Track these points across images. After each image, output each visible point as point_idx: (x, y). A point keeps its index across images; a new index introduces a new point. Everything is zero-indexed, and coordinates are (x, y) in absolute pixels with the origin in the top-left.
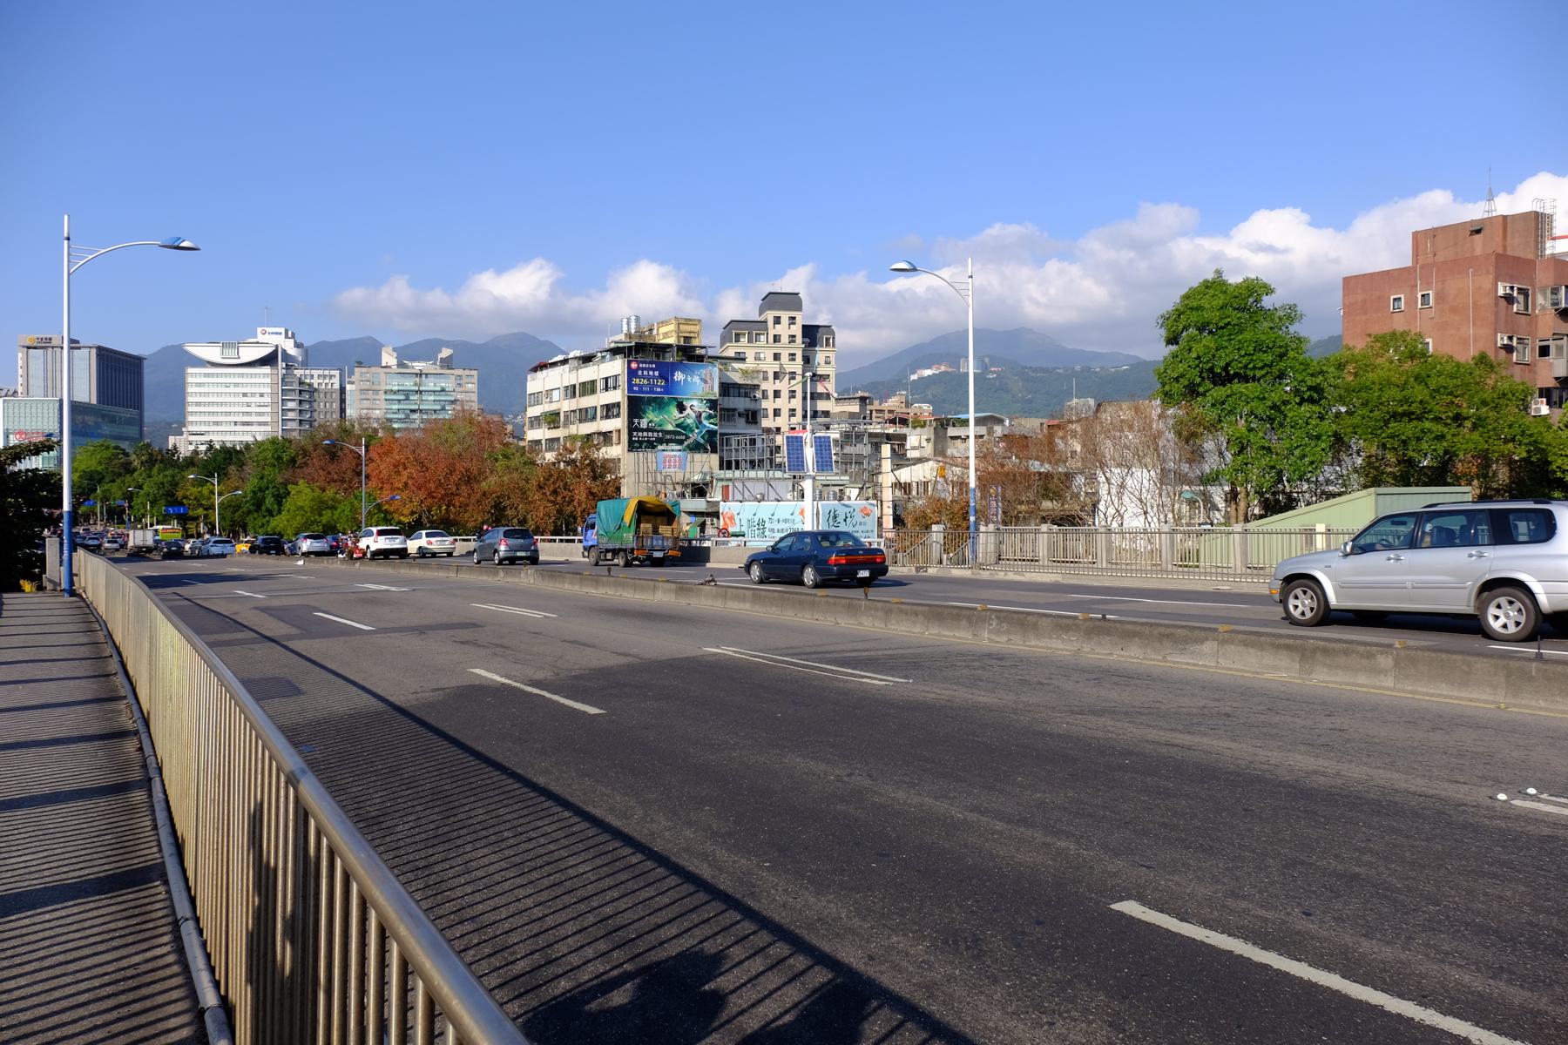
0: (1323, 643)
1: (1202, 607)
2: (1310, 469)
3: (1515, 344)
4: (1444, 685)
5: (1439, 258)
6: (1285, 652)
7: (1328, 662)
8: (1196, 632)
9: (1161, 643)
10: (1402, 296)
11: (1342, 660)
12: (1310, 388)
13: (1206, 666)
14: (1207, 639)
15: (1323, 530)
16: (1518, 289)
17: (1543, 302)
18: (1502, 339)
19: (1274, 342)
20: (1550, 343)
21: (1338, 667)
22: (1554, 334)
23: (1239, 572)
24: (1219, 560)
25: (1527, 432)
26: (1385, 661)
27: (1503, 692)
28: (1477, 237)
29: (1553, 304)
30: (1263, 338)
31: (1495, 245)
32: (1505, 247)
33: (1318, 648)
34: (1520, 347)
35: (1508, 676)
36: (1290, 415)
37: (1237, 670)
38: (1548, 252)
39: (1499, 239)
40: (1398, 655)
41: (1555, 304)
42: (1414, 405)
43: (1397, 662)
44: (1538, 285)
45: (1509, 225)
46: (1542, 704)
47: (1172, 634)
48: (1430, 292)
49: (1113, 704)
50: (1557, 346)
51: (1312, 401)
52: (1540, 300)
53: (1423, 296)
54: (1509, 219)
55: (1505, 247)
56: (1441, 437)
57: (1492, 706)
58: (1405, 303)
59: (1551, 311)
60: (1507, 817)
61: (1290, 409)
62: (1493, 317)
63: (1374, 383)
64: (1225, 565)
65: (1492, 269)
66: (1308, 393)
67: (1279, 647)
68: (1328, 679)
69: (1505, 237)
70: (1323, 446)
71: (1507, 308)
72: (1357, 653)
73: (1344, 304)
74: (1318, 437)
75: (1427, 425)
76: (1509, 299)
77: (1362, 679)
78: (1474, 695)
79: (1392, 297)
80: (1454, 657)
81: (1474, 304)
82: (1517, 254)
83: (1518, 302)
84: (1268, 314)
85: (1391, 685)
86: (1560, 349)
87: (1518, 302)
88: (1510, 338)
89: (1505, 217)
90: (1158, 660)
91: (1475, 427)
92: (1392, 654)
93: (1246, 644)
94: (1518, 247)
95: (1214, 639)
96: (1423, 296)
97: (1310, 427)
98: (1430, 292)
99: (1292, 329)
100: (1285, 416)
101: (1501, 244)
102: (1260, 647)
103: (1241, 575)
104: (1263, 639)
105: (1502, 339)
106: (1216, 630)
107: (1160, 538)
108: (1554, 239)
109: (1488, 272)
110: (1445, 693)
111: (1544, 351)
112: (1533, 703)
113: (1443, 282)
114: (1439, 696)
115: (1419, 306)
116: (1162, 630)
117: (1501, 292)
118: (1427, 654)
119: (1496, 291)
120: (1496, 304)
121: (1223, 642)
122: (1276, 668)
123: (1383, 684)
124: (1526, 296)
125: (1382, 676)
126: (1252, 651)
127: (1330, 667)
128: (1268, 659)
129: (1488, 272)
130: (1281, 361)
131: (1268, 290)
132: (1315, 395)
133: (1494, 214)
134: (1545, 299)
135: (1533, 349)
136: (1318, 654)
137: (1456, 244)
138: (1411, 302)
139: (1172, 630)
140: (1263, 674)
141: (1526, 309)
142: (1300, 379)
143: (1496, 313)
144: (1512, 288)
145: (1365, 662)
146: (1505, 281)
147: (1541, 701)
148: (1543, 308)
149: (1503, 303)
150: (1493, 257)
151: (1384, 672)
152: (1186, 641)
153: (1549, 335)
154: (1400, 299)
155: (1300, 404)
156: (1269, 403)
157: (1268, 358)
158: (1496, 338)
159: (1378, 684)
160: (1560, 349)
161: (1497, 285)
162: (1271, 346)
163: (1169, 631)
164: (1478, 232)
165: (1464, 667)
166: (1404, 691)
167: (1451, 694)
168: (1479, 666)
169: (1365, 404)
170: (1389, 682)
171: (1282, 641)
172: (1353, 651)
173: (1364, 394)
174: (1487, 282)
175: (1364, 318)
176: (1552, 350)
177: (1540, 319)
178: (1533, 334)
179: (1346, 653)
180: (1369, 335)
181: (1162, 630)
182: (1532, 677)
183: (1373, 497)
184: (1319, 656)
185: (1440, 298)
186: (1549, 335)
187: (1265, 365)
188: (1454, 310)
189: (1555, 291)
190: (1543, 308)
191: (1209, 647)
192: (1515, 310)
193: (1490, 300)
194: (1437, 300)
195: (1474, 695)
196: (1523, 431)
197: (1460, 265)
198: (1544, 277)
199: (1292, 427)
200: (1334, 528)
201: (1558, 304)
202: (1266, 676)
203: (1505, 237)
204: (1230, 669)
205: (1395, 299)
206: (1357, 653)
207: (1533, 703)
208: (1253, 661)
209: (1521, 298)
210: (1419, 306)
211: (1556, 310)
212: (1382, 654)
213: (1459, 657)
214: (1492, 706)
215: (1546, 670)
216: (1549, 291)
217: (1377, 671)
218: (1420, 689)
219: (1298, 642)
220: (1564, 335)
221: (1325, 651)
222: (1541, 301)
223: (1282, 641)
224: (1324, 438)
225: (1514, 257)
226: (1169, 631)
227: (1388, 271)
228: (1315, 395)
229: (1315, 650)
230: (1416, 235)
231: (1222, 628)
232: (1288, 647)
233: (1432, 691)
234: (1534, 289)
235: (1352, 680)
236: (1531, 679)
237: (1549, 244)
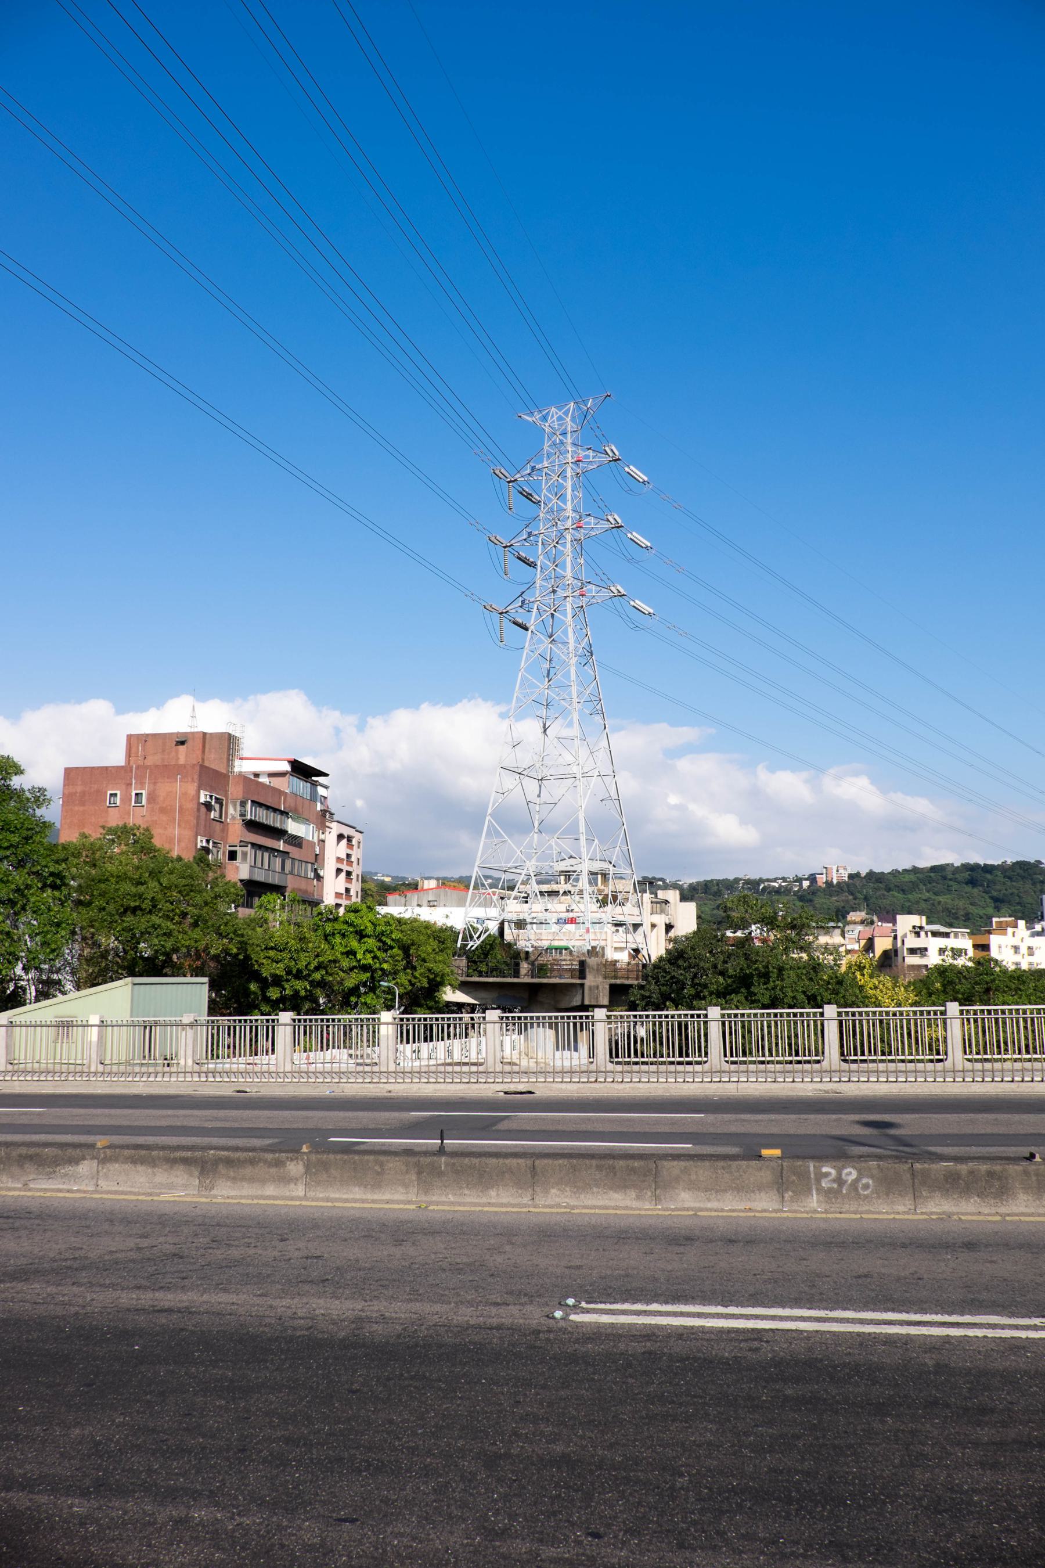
0: (226, 1153)
1: (536, 1119)
2: (51, 957)
3: (211, 847)
4: (357, 1189)
5: (149, 762)
6: (182, 1167)
7: (232, 1174)
8: (70, 1151)
9: (21, 1166)
10: (118, 792)
11: (248, 1171)
12: (52, 874)
13: (85, 1192)
14: (84, 1159)
15: (97, 1022)
16: (216, 798)
17: (233, 813)
18: (202, 841)
19: (23, 824)
20: (238, 849)
21: (243, 1179)
22: (241, 841)
23: (93, 1069)
24: (79, 1056)
25: (239, 932)
26: (295, 1168)
27: (415, 1190)
28: (181, 748)
29: (241, 815)
30: (12, 817)
31: (196, 758)
32: (203, 759)
33: (220, 1159)
34: (215, 850)
35: (419, 1173)
36: (32, 899)
37: (122, 1193)
38: (236, 770)
39: (199, 753)
40: (308, 1160)
41: (243, 815)
42: (146, 901)
43: (308, 1167)
44: (230, 797)
45: (207, 741)
46: (451, 1198)
47: (37, 1155)
48: (143, 792)
49: (23, 1261)
50: (242, 852)
51: (54, 887)
52: (231, 810)
53: (137, 794)
54: (208, 736)
55: (203, 759)
56: (168, 934)
57: (413, 1207)
58: (121, 800)
59: (239, 821)
60: (563, 1330)
61: (32, 894)
62: (195, 821)
63: (112, 876)
64: (78, 1062)
65: (196, 777)
66: (51, 879)
67: (173, 1162)
68: (232, 1193)
69: (203, 752)
70: (63, 933)
71: (206, 814)
72: (265, 1161)
73: (64, 794)
74: (58, 925)
75: (156, 919)
76: (208, 806)
77: (270, 1190)
78: (387, 1196)
79: (109, 792)
80: (366, 1157)
81: (180, 807)
82: (213, 766)
83: (215, 810)
84: (17, 795)
85: (301, 1193)
86: (245, 854)
87: (215, 810)
88: (208, 841)
89: (205, 734)
90: (20, 1189)
91: (195, 925)
92: (302, 1160)
93: (134, 1161)
94: (214, 762)
95: (93, 1158)
96: (137, 794)
97: (52, 913)
98: (143, 792)
99: (39, 812)
100: (28, 900)
101: (200, 757)
102: (151, 1163)
103: (95, 1073)
104: (154, 1153)
105: (202, 841)
106: (92, 1146)
107: (112, 1030)
108: (241, 759)
109: (193, 781)
110: (358, 1197)
111: (233, 856)
112: (443, 1199)
113: (155, 783)
114: (355, 1201)
115: (133, 804)
116: (23, 1151)
117: (202, 800)
118: (339, 1157)
119: (199, 798)
120: (198, 810)
121: (104, 1161)
122: (171, 1186)
123: (294, 1194)
124: (221, 805)
125: (292, 1186)
126: (141, 1168)
127: (234, 1179)
128: (161, 1176)
129: (193, 781)
130: (27, 843)
131: (19, 771)
132: (58, 882)
133: (196, 730)
134: (235, 810)
135: (224, 853)
136: (221, 1167)
137: (163, 751)
138: (126, 799)
139: (38, 1150)
140: (158, 1195)
141: (221, 816)
142: (44, 863)
143: (198, 818)
144: (211, 797)
145: (273, 1170)
146: (205, 790)
147: (450, 1196)
148: (233, 818)
149: (203, 809)
150: (198, 768)
151: (295, 1180)
152: (56, 1162)
153: (237, 842)
154: (116, 795)
155: (43, 889)
156: (13, 887)
157: (15, 839)
158: (196, 839)
159: (288, 1194)
160: (245, 854)
161: (199, 792)
162: (18, 827)
163: (32, 1151)
164: (183, 743)
165: (377, 1168)
166: (317, 1200)
167: (364, 1197)
168: (391, 1165)
169: (103, 894)
170: (300, 1190)
171: (178, 1154)
172: (260, 1160)
173: (102, 886)
174: (192, 788)
175: (81, 809)
176: (239, 856)
177: (230, 826)
178: (224, 839)
179: (252, 1162)
180: (103, 827)
181: (23, 1151)
182: (442, 1172)
183: (130, 986)
184: (221, 1168)
185: (152, 798)
186: (237, 842)
187: (11, 845)
188: (163, 810)
189: (243, 804)
190: (233, 818)
191: (86, 1167)
192: (212, 817)
193: (191, 806)
194: (149, 800)
195: (387, 1196)
196: (236, 931)
197: (168, 771)
198: (235, 791)
199: (34, 912)
200: (108, 1020)
201: (245, 815)
202: (162, 1198)
203: (203, 752)
204: (116, 1192)
205: (111, 795)
206: (265, 1161)
207: (443, 1199)
208: (141, 1180)
209: (217, 807)
210: (133, 804)
211: (243, 821)
212: (292, 1160)
213: (371, 1158)
214: (413, 1207)
215: (454, 1164)
216: (238, 804)
217: (286, 1180)
218: (332, 1195)
219: (198, 1154)
220: (249, 843)
221: (229, 1162)
222: (232, 811)
223: (178, 1154)
224: (64, 925)
225: (214, 770)
226: (32, 1151)
227: (107, 768)
228: (58, 882)
229: (217, 1161)
230: (130, 737)
231: (101, 1141)
232: (185, 1161)
233: (345, 1196)
234: (227, 799)
235: (259, 1193)
236: (440, 1174)
237: (237, 762)
